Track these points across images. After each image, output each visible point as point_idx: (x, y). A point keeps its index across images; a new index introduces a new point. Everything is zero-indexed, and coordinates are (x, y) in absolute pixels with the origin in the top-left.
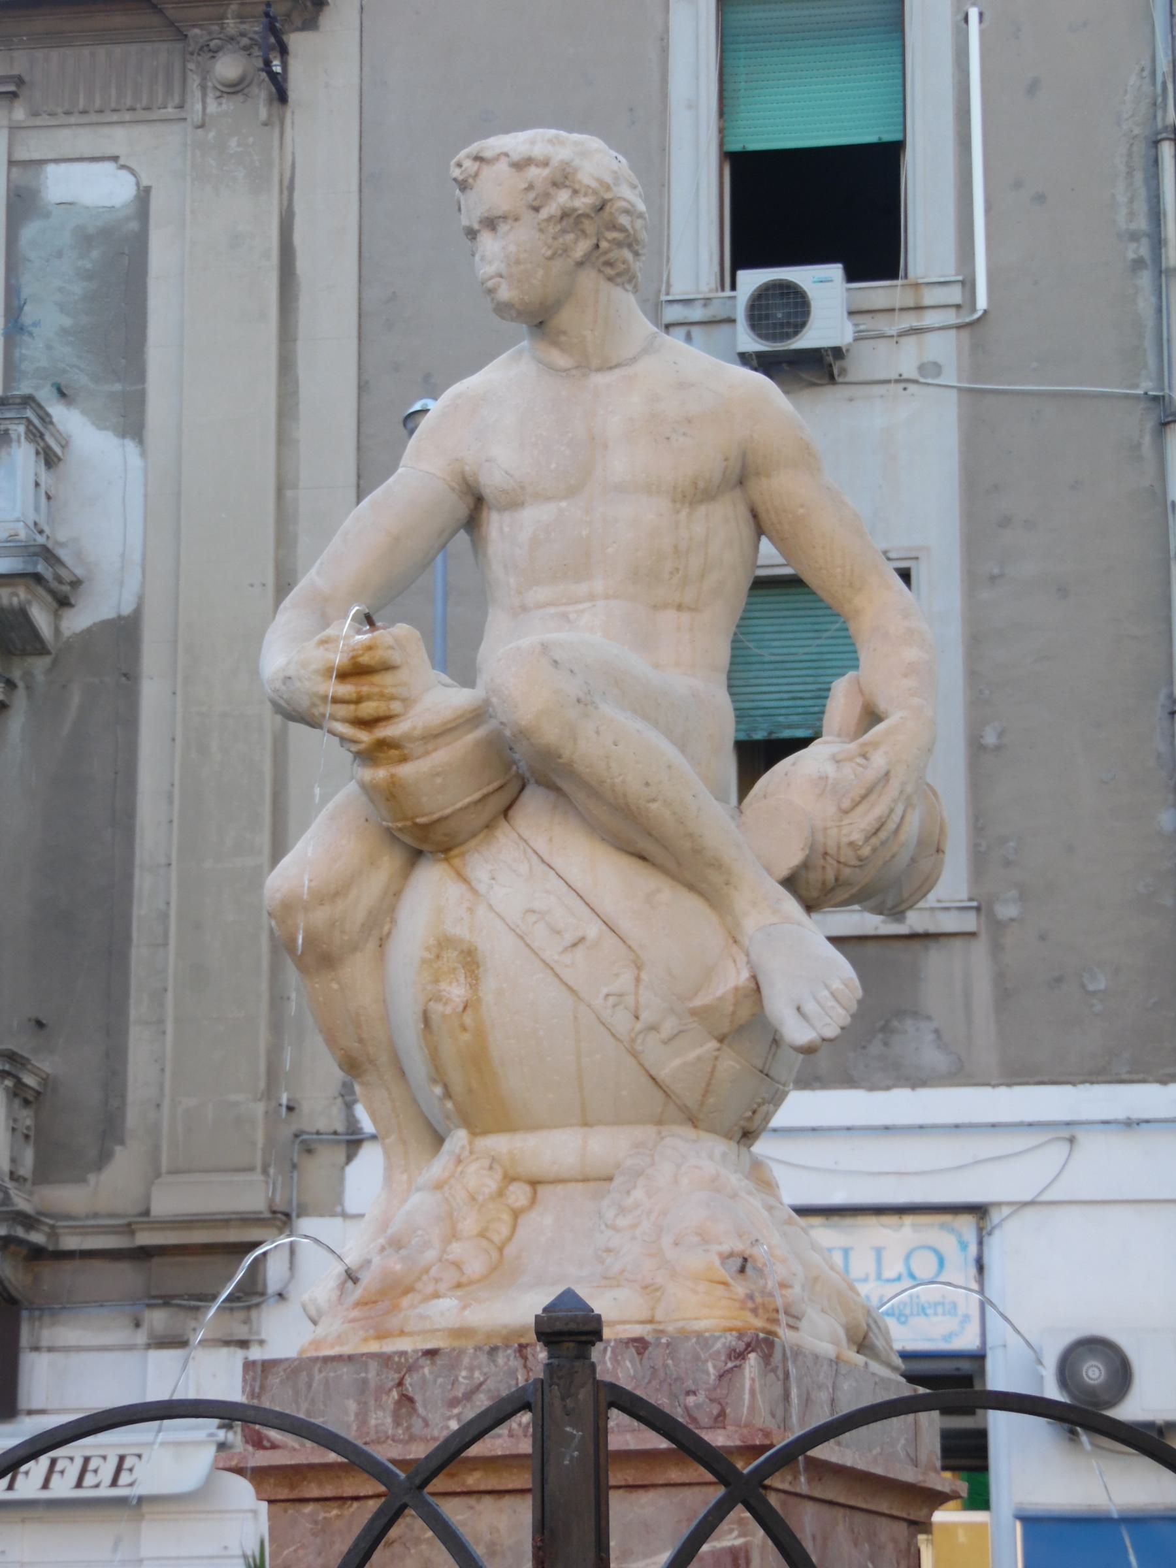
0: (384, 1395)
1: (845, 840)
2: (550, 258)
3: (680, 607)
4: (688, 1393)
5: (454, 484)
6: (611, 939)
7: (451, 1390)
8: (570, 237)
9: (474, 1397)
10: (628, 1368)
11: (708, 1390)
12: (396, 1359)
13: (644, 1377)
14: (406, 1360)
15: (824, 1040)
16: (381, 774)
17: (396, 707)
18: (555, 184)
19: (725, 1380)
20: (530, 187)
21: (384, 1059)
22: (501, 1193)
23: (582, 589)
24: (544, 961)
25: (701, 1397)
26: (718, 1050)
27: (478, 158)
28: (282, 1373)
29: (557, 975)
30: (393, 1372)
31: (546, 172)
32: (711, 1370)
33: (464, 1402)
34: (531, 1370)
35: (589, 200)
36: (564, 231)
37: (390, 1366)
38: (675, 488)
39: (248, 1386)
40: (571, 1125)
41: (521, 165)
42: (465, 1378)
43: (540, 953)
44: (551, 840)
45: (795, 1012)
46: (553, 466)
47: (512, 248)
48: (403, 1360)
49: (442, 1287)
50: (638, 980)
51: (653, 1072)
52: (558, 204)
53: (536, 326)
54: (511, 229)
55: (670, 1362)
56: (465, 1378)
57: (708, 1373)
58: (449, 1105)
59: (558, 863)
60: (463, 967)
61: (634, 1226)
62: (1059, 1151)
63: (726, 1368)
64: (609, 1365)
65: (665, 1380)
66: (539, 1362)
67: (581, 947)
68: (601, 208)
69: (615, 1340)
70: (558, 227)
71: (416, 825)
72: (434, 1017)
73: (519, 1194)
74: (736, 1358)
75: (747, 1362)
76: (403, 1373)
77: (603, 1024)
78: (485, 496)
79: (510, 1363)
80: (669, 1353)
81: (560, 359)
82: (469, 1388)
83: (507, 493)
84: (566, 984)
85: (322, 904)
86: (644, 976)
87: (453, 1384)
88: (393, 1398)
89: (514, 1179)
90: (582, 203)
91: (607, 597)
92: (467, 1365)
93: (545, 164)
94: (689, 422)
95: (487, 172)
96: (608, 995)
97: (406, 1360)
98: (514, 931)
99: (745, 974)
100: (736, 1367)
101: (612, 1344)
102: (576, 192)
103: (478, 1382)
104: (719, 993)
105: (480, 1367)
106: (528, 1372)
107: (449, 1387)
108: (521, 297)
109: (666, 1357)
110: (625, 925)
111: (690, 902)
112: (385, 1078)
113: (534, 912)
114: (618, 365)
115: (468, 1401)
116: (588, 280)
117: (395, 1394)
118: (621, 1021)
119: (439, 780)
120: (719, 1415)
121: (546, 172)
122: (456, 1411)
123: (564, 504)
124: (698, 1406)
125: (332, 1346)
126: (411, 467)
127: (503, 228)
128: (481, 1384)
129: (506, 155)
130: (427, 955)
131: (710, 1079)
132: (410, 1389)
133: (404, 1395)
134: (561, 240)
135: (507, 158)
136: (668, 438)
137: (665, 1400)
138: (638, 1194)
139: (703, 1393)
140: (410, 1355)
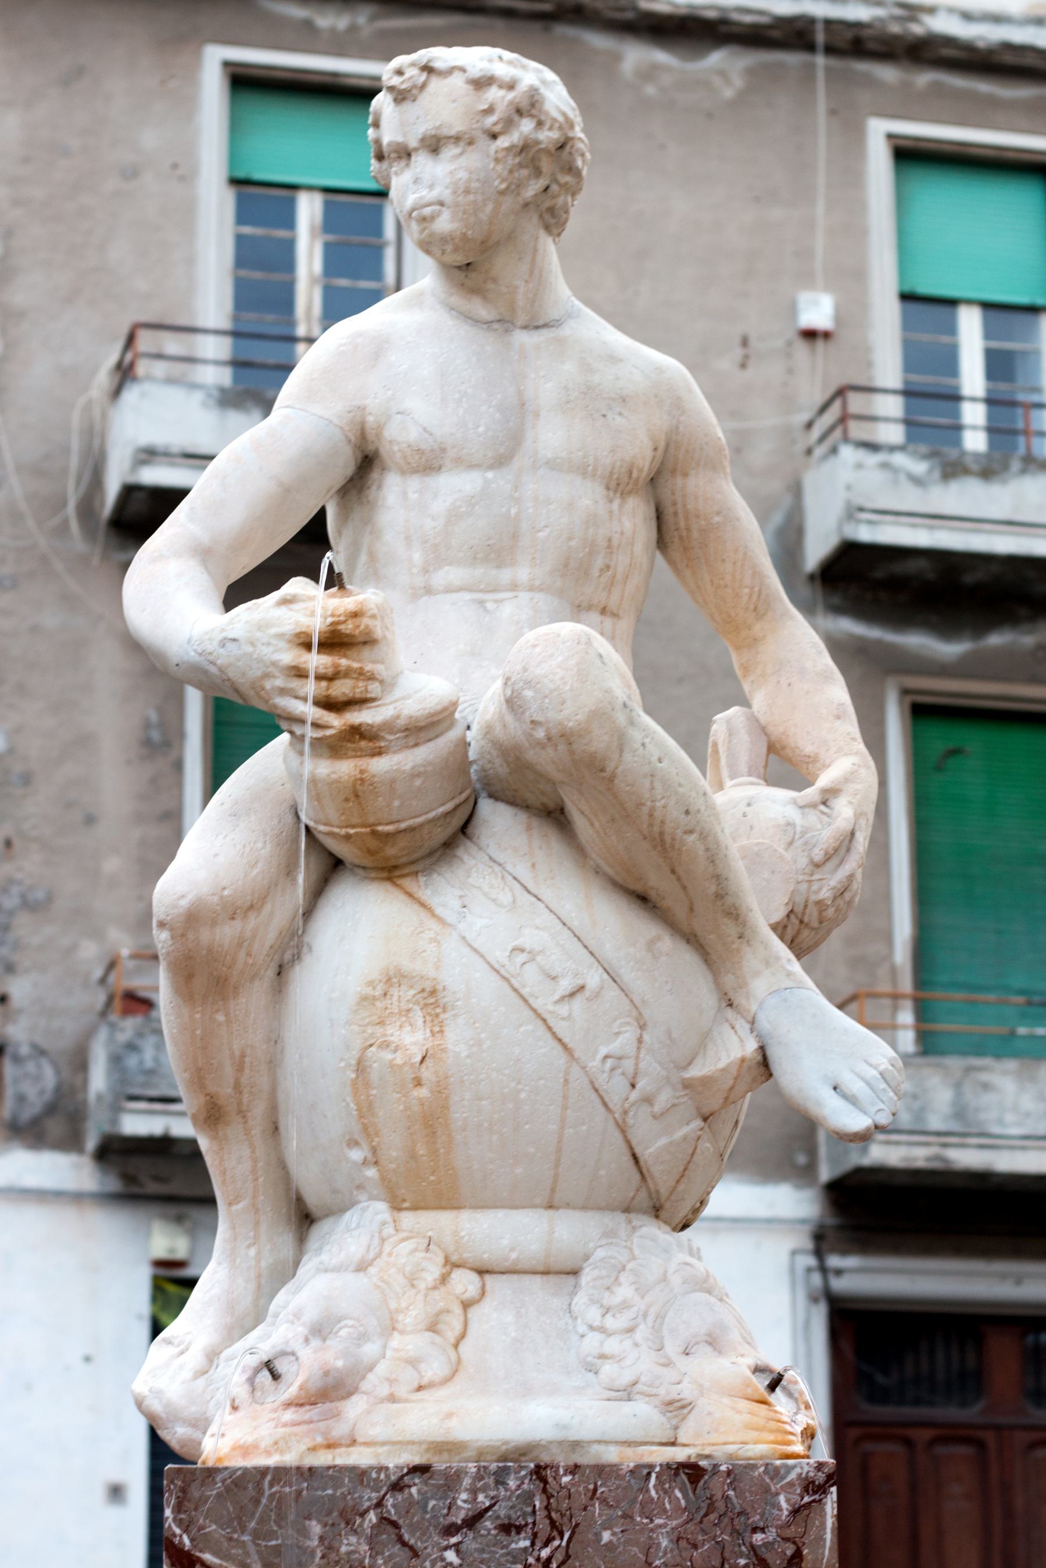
0: (357, 1517)
1: (814, 898)
2: (502, 193)
3: (603, 611)
4: (755, 1530)
5: (350, 435)
6: (612, 993)
7: (448, 1515)
8: (524, 172)
9: (478, 1525)
10: (678, 1499)
11: (781, 1527)
12: (374, 1475)
13: (698, 1509)
14: (387, 1476)
15: (876, 1127)
16: (345, 768)
17: (374, 689)
18: (519, 112)
19: (800, 1517)
20: (490, 111)
21: (258, 1111)
22: (444, 1279)
23: (505, 575)
24: (534, 1010)
25: (772, 1535)
26: (702, 1129)
27: (428, 69)
28: (220, 1485)
29: (550, 1028)
30: (369, 1491)
31: (511, 96)
32: (784, 1505)
33: (465, 1530)
34: (553, 1496)
35: (555, 135)
36: (521, 165)
37: (365, 1483)
38: (611, 473)
39: (174, 1497)
40: (535, 1206)
41: (482, 83)
42: (465, 1501)
43: (531, 1001)
44: (533, 865)
45: (832, 1092)
46: (481, 429)
47: (463, 175)
48: (382, 1476)
49: (402, 1391)
50: (640, 1041)
51: (638, 1151)
52: (521, 133)
53: (459, 268)
54: (461, 154)
55: (731, 1493)
56: (465, 1501)
57: (780, 1509)
58: (371, 1173)
59: (546, 893)
60: (422, 1009)
61: (630, 1330)
62: (423, 1384)
63: (802, 1503)
64: (653, 1493)
65: (725, 1514)
66: (561, 1488)
67: (579, 997)
68: (562, 147)
69: (661, 1465)
70: (517, 160)
71: (374, 833)
72: (375, 1070)
73: (465, 1282)
74: (815, 1492)
75: (829, 1496)
76: (382, 1493)
77: (597, 1091)
78: (383, 452)
79: (525, 1486)
80: (731, 1483)
81: (483, 311)
82: (470, 1513)
83: (423, 453)
84: (560, 1040)
85: (233, 919)
86: (646, 1037)
87: (449, 1508)
88: (370, 1520)
89: (457, 1266)
90: (548, 136)
91: (531, 589)
92: (468, 1487)
93: (511, 86)
94: (624, 401)
95: (436, 84)
96: (606, 1057)
97: (387, 1476)
98: (498, 972)
99: (751, 1046)
100: (814, 1501)
101: (657, 1469)
102: (540, 124)
103: (483, 1507)
104: (721, 1065)
105: (484, 1489)
106: (549, 1498)
107: (445, 1511)
108: (464, 230)
109: (726, 1487)
110: (629, 975)
111: (688, 957)
112: (253, 1132)
113: (523, 950)
114: (545, 326)
115: (470, 1529)
116: (531, 225)
117: (372, 1517)
118: (616, 1088)
119: (418, 782)
120: (793, 1557)
121: (511, 96)
122: (454, 1540)
123: (490, 475)
124: (766, 1545)
125: (268, 1453)
126: (300, 410)
127: (450, 151)
128: (487, 1509)
129: (463, 70)
130: (369, 991)
131: (689, 1162)
132: (393, 1511)
133: (386, 1519)
134: (516, 175)
135: (461, 73)
136: (604, 416)
137: (726, 1537)
138: (625, 1291)
139: (774, 1530)
140: (391, 1471)
